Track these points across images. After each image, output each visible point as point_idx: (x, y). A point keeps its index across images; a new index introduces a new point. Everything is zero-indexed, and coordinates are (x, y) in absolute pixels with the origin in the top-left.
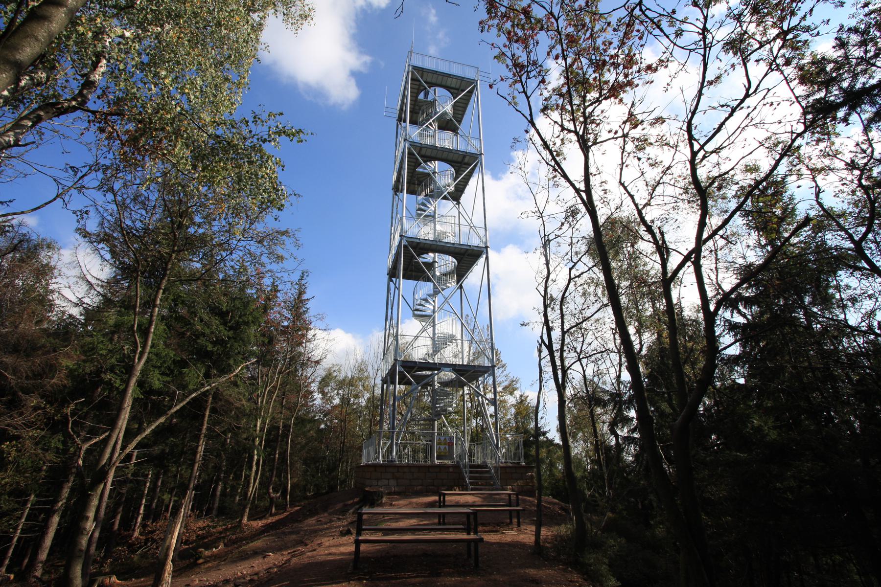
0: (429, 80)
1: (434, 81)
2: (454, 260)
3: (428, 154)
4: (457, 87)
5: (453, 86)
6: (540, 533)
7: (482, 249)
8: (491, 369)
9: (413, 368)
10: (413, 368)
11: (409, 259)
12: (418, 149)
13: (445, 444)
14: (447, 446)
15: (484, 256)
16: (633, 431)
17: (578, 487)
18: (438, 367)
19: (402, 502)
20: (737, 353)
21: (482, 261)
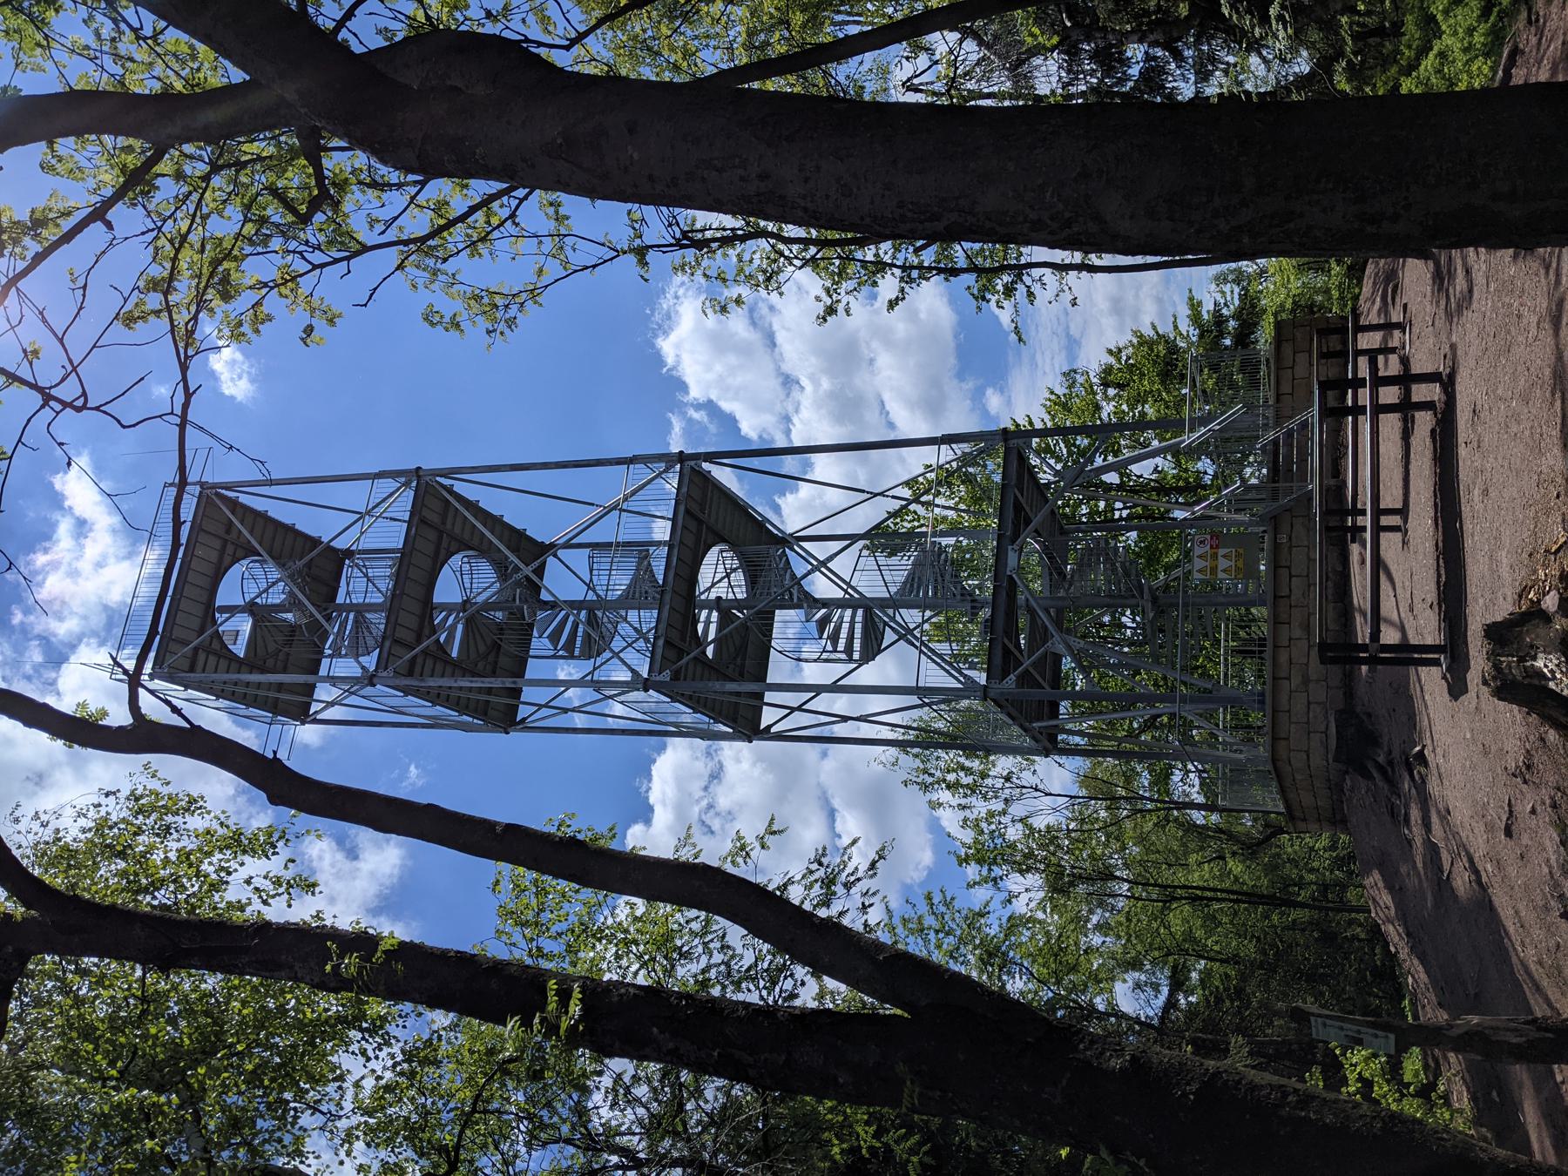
0: (195, 623)
1: (198, 610)
2: (715, 550)
3: (411, 621)
4: (217, 544)
5: (214, 556)
6: (782, 58)
7: (687, 471)
8: (1013, 443)
9: (1007, 652)
10: (1007, 652)
11: (713, 669)
12: (397, 650)
13: (1215, 556)
14: (1222, 552)
15: (706, 466)
16: (1178, 56)
17: (122, 180)
18: (1007, 587)
19: (1548, 1143)
20: (1397, 642)
21: (723, 475)
